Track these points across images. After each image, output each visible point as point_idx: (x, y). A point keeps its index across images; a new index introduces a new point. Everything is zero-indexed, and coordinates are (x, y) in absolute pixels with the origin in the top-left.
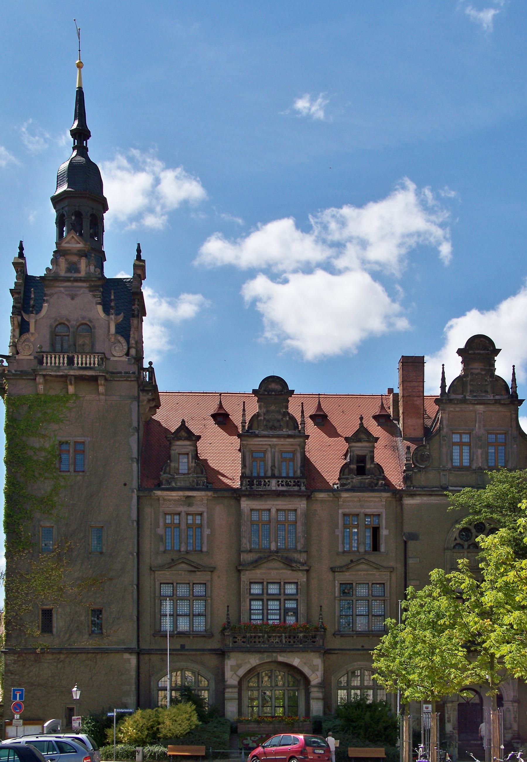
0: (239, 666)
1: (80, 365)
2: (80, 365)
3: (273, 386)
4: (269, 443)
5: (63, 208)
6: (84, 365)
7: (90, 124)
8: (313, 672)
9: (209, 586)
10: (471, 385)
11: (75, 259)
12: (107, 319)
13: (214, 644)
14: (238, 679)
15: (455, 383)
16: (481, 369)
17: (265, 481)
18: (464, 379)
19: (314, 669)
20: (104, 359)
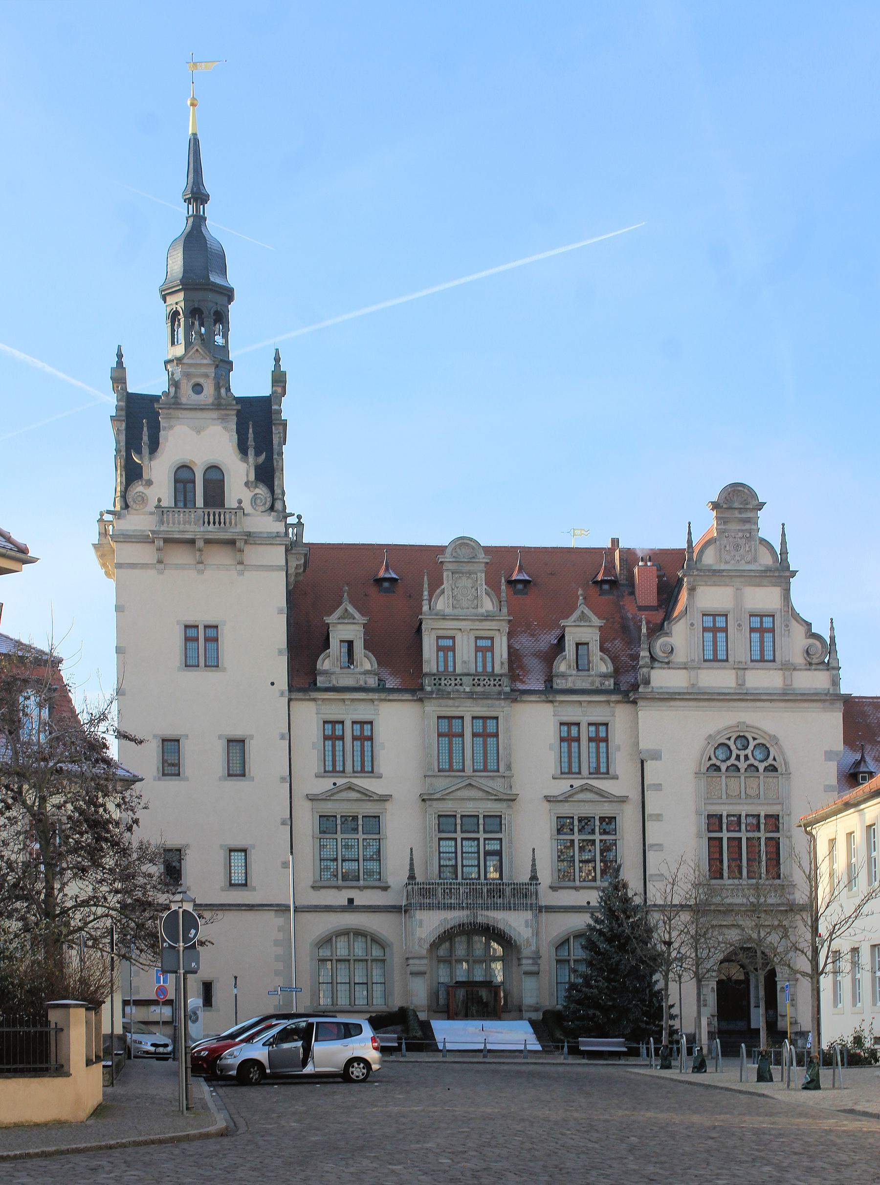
5: (177, 303)
7: (209, 184)
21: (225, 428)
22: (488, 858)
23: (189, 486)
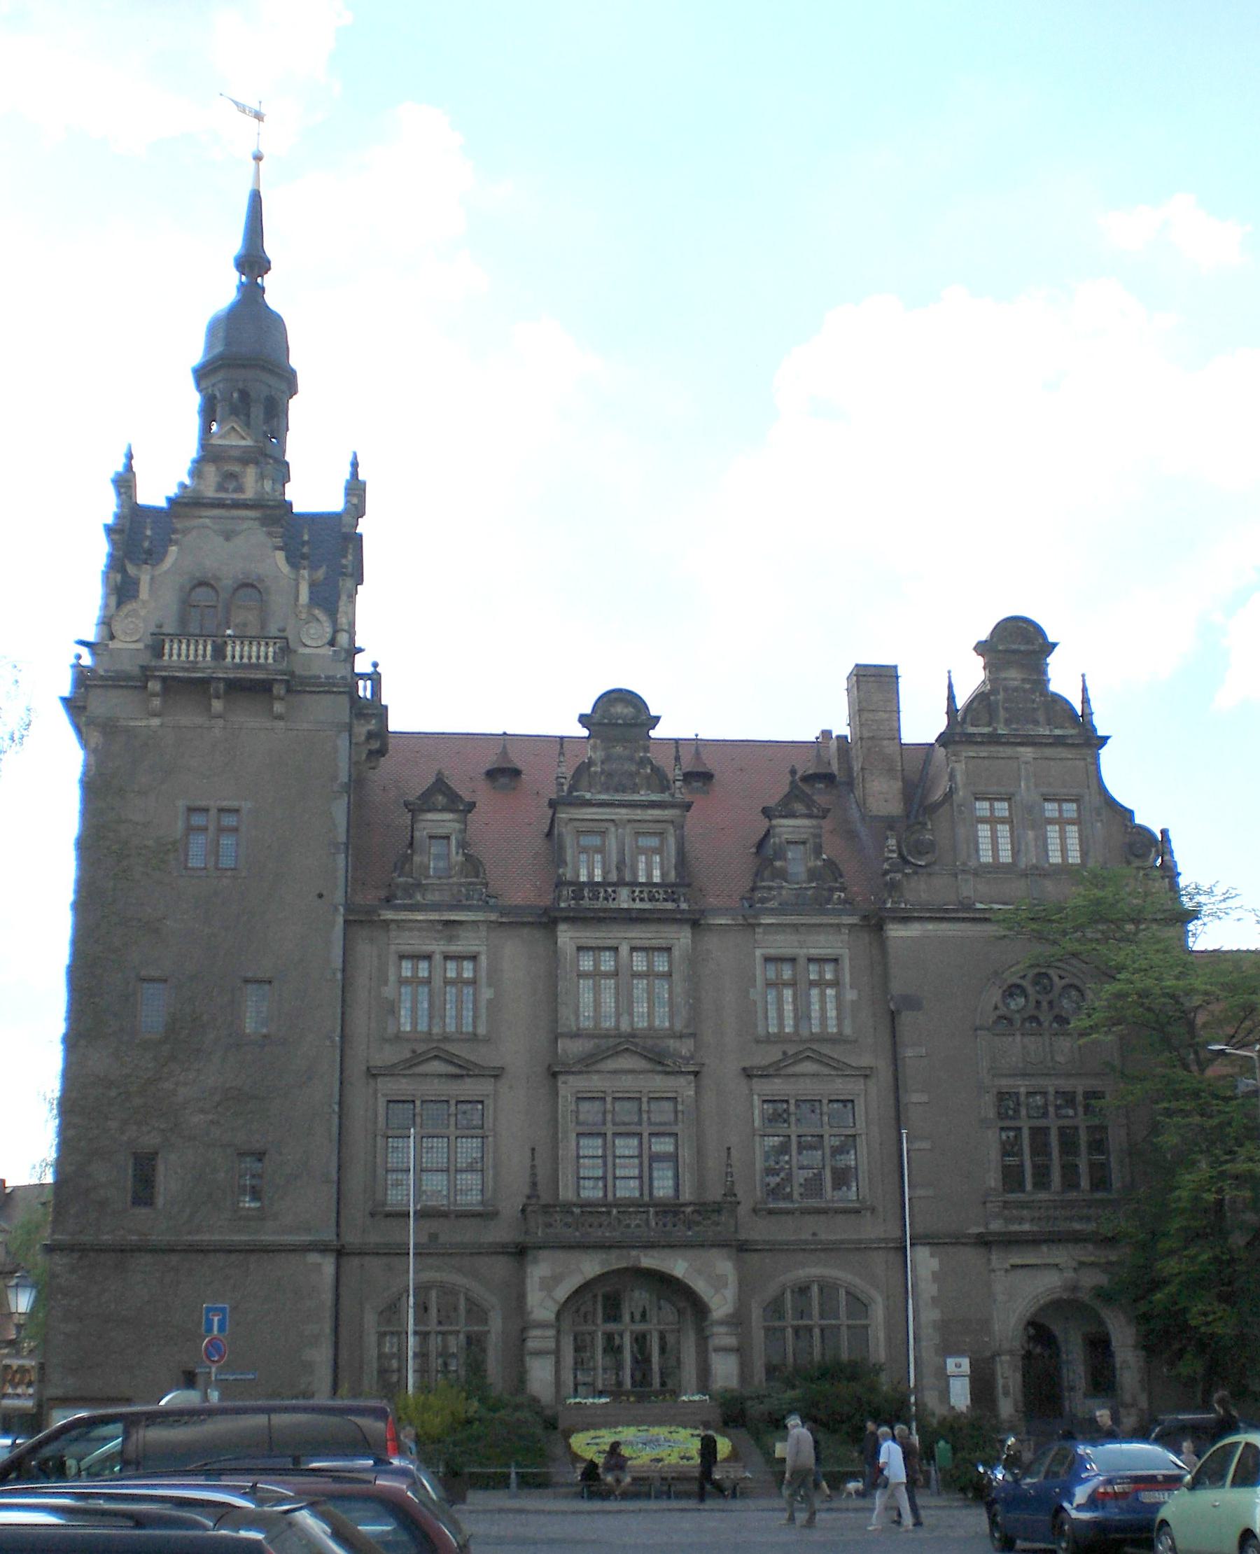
0: (557, 1279)
1: (237, 660)
2: (237, 660)
3: (619, 709)
4: (613, 817)
5: (213, 385)
6: (245, 660)
8: (717, 1291)
9: (491, 1108)
10: (1006, 709)
11: (236, 468)
12: (293, 576)
13: (500, 1233)
14: (555, 1308)
15: (975, 704)
16: (1023, 680)
17: (606, 891)
18: (992, 698)
19: (718, 1283)
20: (286, 650)
21: (984, 682)
22: (655, 1165)
23: (404, 1336)
